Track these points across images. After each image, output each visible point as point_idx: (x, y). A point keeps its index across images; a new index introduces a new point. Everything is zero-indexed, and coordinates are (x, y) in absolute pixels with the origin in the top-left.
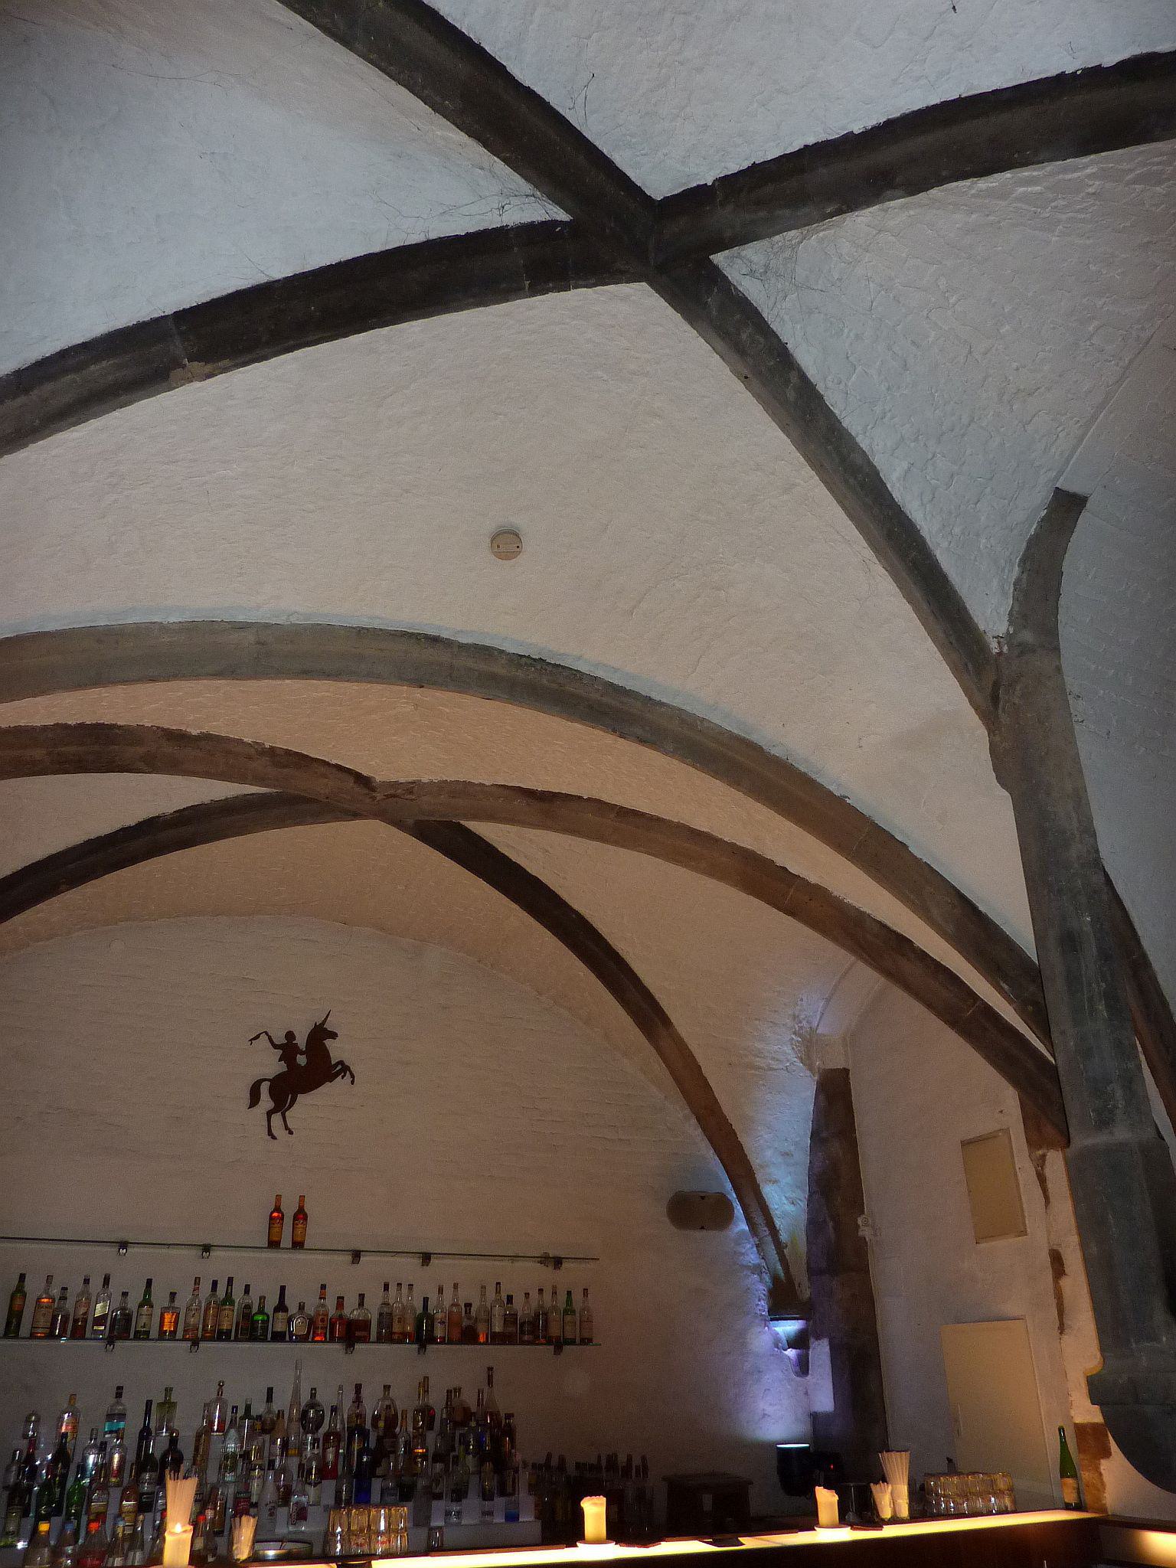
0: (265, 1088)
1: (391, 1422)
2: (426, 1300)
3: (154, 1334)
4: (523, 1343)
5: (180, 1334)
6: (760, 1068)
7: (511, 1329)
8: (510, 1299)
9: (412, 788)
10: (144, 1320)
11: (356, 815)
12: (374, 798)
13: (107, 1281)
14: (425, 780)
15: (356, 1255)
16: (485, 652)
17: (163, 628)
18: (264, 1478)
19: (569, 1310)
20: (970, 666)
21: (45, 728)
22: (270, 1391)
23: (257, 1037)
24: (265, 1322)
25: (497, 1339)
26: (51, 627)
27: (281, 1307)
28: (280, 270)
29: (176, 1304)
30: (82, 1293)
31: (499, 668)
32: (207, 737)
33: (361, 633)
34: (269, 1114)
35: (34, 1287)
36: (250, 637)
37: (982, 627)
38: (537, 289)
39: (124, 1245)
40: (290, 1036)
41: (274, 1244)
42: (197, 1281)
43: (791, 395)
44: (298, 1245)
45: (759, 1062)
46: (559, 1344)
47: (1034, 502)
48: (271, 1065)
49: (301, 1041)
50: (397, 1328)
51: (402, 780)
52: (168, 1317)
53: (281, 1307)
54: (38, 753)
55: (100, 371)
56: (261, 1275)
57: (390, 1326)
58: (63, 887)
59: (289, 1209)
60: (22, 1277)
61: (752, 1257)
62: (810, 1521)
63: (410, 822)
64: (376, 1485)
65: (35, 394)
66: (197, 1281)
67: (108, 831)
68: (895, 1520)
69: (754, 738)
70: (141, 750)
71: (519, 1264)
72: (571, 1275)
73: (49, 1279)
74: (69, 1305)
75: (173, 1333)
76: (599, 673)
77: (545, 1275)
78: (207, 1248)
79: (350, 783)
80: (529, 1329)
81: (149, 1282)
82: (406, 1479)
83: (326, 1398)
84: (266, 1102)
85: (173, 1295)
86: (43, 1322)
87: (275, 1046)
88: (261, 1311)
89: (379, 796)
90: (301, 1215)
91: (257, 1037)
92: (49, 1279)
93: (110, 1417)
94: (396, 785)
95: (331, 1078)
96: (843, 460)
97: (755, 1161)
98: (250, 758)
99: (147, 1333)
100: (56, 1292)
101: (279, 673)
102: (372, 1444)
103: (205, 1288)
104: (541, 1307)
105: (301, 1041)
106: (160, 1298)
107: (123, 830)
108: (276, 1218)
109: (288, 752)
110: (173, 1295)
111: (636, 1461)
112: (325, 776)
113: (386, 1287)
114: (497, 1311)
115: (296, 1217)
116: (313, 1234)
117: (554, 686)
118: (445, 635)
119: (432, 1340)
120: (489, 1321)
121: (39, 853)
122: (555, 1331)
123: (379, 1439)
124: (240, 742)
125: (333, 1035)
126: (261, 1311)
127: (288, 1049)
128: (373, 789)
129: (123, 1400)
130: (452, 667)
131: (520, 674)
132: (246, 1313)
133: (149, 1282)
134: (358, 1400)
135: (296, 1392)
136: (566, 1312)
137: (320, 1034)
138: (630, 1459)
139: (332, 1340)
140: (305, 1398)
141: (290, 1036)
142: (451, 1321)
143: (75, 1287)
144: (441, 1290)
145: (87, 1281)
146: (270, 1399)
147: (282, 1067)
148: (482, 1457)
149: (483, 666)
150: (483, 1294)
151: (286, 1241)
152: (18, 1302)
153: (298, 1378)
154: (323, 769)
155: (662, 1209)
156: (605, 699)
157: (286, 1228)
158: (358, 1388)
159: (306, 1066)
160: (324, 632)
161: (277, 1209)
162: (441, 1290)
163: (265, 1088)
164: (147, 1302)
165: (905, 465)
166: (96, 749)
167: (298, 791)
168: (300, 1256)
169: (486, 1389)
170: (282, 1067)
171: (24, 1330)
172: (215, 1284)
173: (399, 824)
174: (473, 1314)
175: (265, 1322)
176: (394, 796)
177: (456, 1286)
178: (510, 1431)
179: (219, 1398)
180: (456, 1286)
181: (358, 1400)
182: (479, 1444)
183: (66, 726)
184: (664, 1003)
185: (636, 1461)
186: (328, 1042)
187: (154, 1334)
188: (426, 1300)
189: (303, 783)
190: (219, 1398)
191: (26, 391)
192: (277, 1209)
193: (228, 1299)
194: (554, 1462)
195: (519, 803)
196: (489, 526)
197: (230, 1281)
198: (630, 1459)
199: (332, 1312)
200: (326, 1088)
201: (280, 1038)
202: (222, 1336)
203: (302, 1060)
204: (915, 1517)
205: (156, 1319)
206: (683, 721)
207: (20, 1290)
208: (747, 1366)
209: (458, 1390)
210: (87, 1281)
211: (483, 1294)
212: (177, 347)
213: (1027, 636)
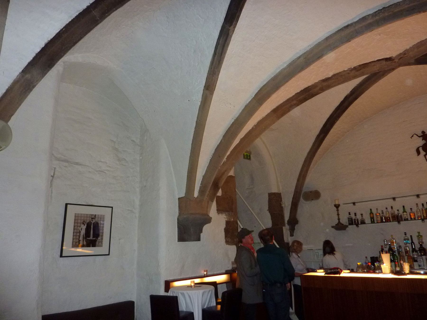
0: (421, 149)
3: (409, 219)
5: (417, 218)
9: (405, 53)
11: (393, 69)
12: (395, 62)
13: (392, 208)
16: (364, 19)
17: (284, 69)
21: (293, 96)
23: (413, 136)
26: (265, 83)
29: (413, 211)
30: (386, 212)
32: (334, 75)
33: (327, 39)
35: (374, 211)
36: (302, 58)
42: (417, 204)
46: (357, 225)
51: (401, 52)
52: (412, 214)
60: (371, 210)
63: (413, 61)
66: (417, 204)
67: (339, 104)
70: (318, 88)
79: (384, 62)
81: (404, 207)
85: (411, 209)
86: (379, 219)
87: (419, 137)
91: (413, 136)
93: (405, 240)
98: (349, 73)
99: (407, 219)
101: (313, 62)
103: (420, 207)
106: (408, 209)
107: (342, 102)
109: (360, 66)
110: (411, 209)
112: (374, 65)
117: (390, 13)
118: (350, 23)
121: (328, 116)
124: (344, 71)
128: (394, 60)
129: (407, 235)
131: (377, 18)
133: (404, 207)
145: (387, 208)
149: (364, 24)
154: (373, 64)
156: (411, 5)
160: (319, 45)
163: (421, 149)
164: (404, 211)
167: (373, 73)
172: (423, 205)
173: (409, 64)
176: (401, 58)
183: (298, 93)
187: (409, 219)
201: (420, 134)
204: (411, 273)
205: (409, 215)
207: (371, 213)
210: (387, 208)
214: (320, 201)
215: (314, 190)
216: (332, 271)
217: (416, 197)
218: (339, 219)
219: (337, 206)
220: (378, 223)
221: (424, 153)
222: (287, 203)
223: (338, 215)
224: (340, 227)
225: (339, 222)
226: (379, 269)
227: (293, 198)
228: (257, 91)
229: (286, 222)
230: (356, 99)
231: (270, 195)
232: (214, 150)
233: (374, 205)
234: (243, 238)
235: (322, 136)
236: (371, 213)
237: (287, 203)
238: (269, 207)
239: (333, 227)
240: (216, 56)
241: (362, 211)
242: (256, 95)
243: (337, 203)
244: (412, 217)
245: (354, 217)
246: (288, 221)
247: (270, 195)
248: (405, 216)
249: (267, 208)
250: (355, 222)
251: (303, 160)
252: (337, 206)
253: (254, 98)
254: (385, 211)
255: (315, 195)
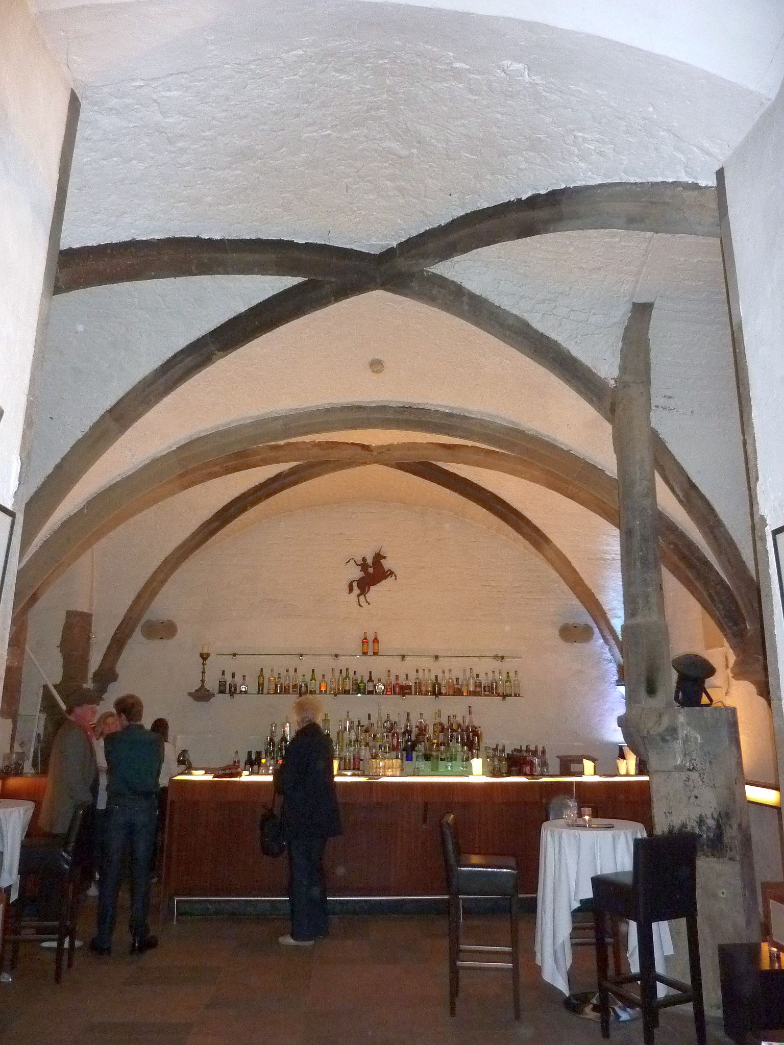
0: (355, 585)
1: (422, 730)
2: (436, 677)
3: (318, 692)
4: (485, 695)
6: (606, 560)
7: (478, 689)
8: (478, 676)
10: (313, 686)
11: (366, 464)
14: (395, 443)
15: (403, 657)
18: (365, 750)
19: (508, 680)
20: (594, 399)
22: (369, 715)
24: (365, 687)
25: (470, 693)
27: (370, 680)
28: (243, 309)
31: (390, 416)
34: (359, 596)
35: (267, 674)
36: (281, 422)
37: (603, 377)
38: (337, 300)
39: (301, 655)
40: (364, 559)
41: (365, 654)
43: (465, 307)
44: (375, 654)
45: (608, 556)
47: (621, 313)
48: (357, 574)
49: (370, 561)
50: (423, 689)
53: (370, 680)
54: (217, 469)
55: (188, 362)
56: (360, 666)
57: (420, 688)
58: (452, 287)
59: (371, 639)
61: (609, 656)
62: (581, 774)
64: (414, 754)
65: (169, 374)
68: (627, 775)
69: (521, 428)
70: (259, 457)
71: (483, 659)
72: (508, 665)
73: (272, 670)
74: (282, 680)
75: (325, 691)
76: (439, 409)
77: (497, 664)
78: (336, 656)
80: (491, 690)
82: (428, 752)
83: (394, 718)
84: (356, 591)
86: (273, 688)
88: (362, 682)
89: (375, 454)
90: (376, 640)
92: (272, 670)
94: (383, 447)
95: (385, 578)
96: (501, 325)
97: (606, 607)
98: (309, 449)
100: (276, 675)
102: (413, 738)
103: (337, 673)
104: (494, 679)
105: (370, 561)
106: (318, 676)
108: (365, 641)
109: (327, 442)
111: (540, 749)
113: (417, 671)
114: (471, 681)
115: (374, 642)
116: (383, 647)
119: (440, 694)
120: (467, 686)
122: (500, 690)
123: (417, 736)
125: (384, 558)
126: (362, 682)
127: (364, 566)
128: (371, 451)
130: (368, 419)
132: (356, 683)
134: (408, 720)
135: (380, 716)
136: (506, 682)
137: (378, 557)
138: (536, 747)
139: (395, 693)
140: (384, 718)
141: (364, 559)
142: (449, 686)
143: (284, 673)
144: (443, 672)
146: (369, 718)
147: (362, 574)
148: (463, 744)
149: (382, 416)
150: (465, 674)
151: (371, 653)
152: (261, 679)
153: (380, 709)
154: (344, 447)
155: (555, 632)
156: (443, 421)
157: (370, 645)
158: (408, 714)
159: (373, 573)
161: (365, 638)
162: (443, 672)
163: (355, 585)
165: (540, 315)
166: (240, 460)
168: (375, 657)
169: (468, 716)
170: (362, 574)
171: (265, 691)
174: (460, 682)
175: (365, 687)
177: (450, 670)
178: (476, 734)
179: (348, 718)
180: (450, 670)
181: (408, 720)
182: (462, 739)
184: (546, 532)
185: (540, 749)
186: (382, 561)
187: (318, 692)
188: (436, 677)
189: (334, 454)
190: (348, 718)
191: (166, 374)
192: (365, 638)
193: (347, 676)
194: (500, 748)
195: (440, 451)
196: (371, 357)
197: (347, 669)
198: (536, 747)
199: (394, 682)
200: (383, 583)
202: (346, 692)
203: (371, 570)
204: (637, 775)
206: (482, 425)
207: (261, 675)
208: (606, 707)
209: (455, 716)
211: (465, 674)
212: (213, 348)
213: (628, 378)
214: (171, 643)
215: (165, 619)
216: (227, 771)
217: (432, 659)
218: (203, 681)
219: (204, 657)
220: (269, 693)
221: (358, 592)
222: (101, 637)
223: (203, 672)
224: (202, 695)
225: (203, 685)
226: (469, 773)
227: (118, 629)
228: (183, 443)
229: (91, 675)
230: (295, 483)
231: (70, 615)
232: (59, 524)
233: (267, 662)
234: (79, 705)
235: (214, 525)
236: (261, 675)
237: (101, 637)
238: (62, 641)
239: (190, 694)
240: (162, 380)
241: (244, 671)
242: (181, 448)
243: (205, 651)
244: (323, 689)
245: (229, 680)
246: (95, 674)
247: (70, 615)
248: (313, 686)
249: (57, 639)
250: (230, 688)
251: (162, 558)
252: (204, 657)
253: (174, 451)
254: (284, 673)
255: (164, 630)
